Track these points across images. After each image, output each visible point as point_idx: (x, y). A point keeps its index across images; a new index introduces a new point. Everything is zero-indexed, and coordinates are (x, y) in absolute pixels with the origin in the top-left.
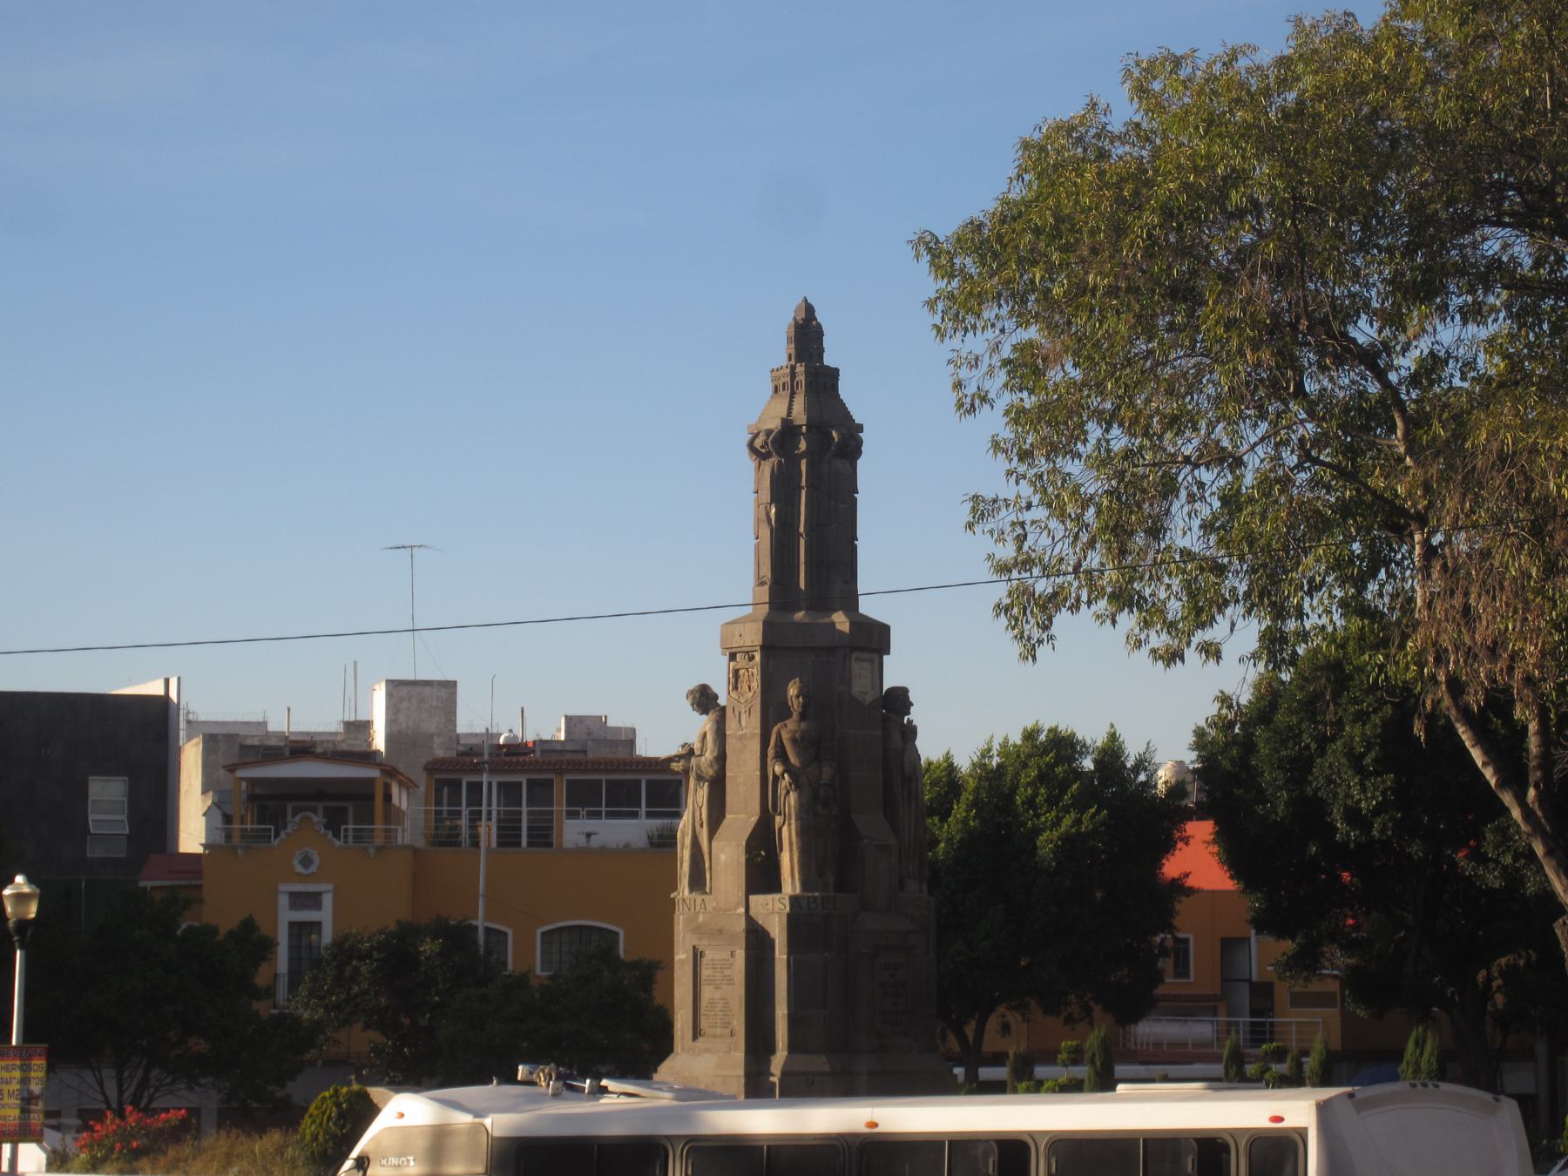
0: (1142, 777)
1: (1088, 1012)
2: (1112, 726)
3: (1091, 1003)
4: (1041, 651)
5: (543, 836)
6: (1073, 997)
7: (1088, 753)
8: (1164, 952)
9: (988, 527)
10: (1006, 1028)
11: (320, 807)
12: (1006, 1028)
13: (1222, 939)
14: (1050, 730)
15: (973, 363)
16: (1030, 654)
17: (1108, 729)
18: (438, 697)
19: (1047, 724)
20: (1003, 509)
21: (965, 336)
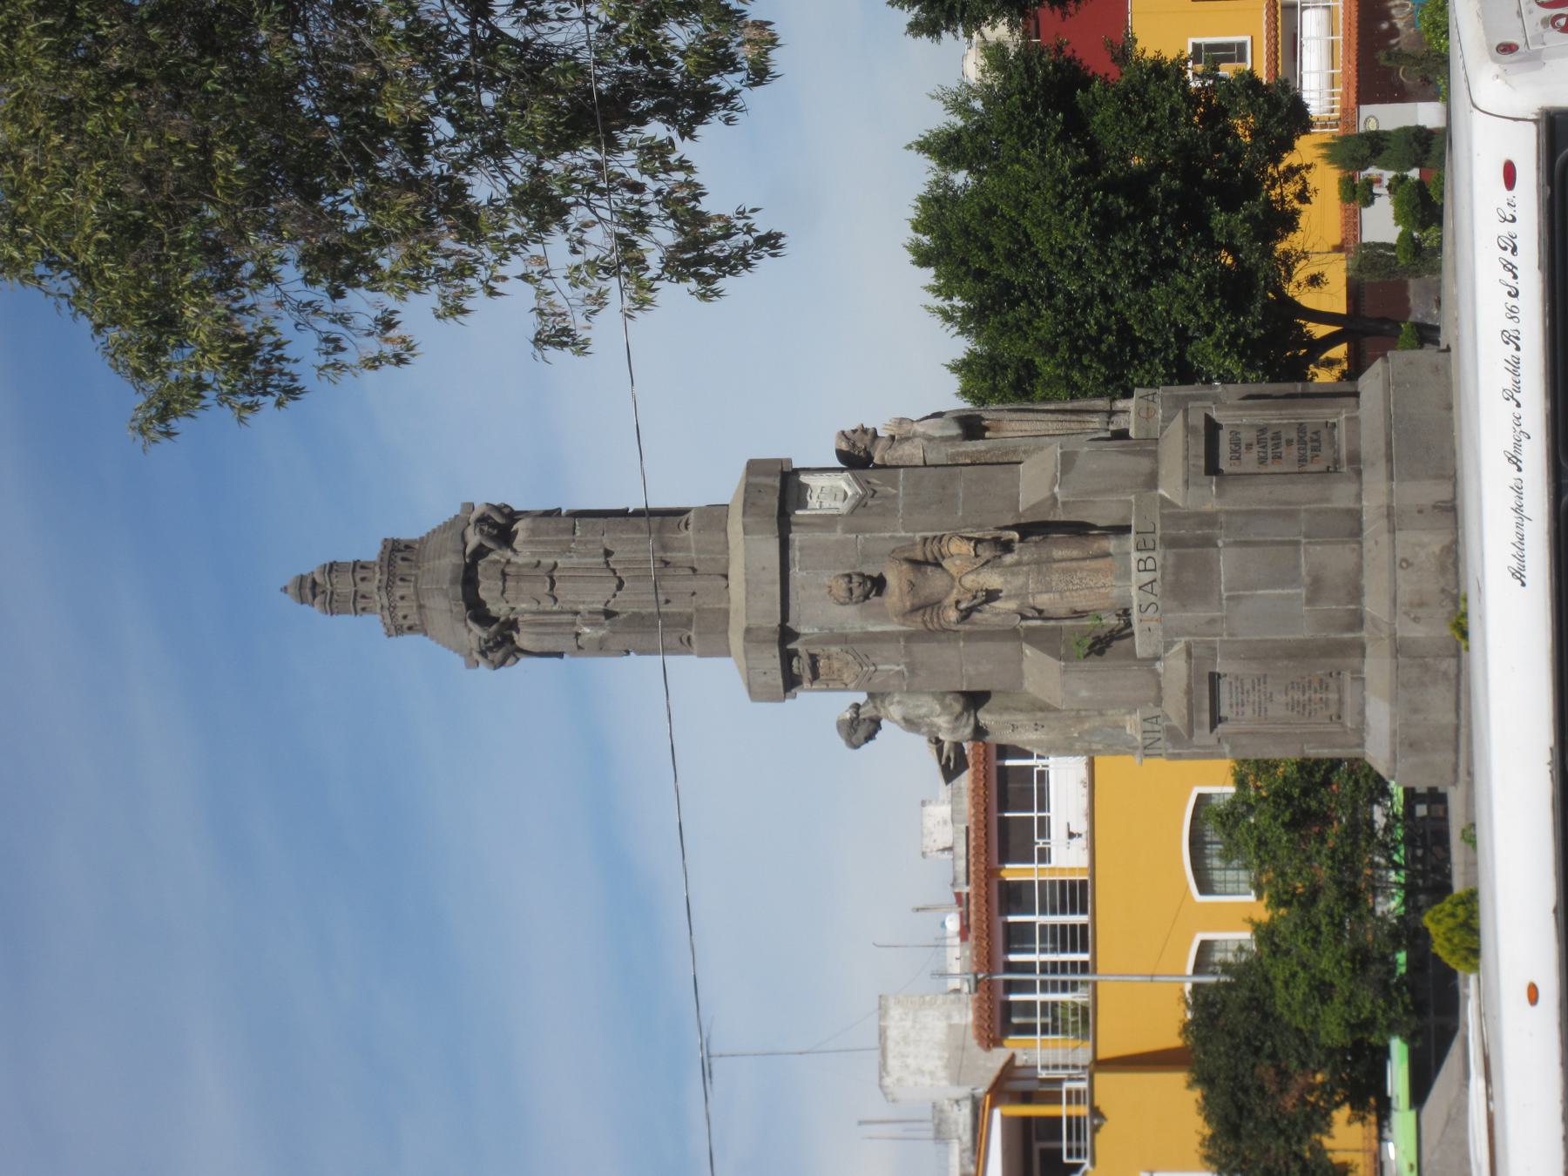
0: (978, 104)
1: (1292, 171)
2: (909, 147)
3: (1282, 167)
5: (1075, 895)
6: (1273, 192)
7: (946, 178)
8: (1211, 73)
9: (581, 321)
10: (1315, 281)
12: (1315, 281)
14: (915, 229)
17: (913, 152)
18: (902, 1019)
19: (908, 235)
20: (555, 298)
21: (288, 360)
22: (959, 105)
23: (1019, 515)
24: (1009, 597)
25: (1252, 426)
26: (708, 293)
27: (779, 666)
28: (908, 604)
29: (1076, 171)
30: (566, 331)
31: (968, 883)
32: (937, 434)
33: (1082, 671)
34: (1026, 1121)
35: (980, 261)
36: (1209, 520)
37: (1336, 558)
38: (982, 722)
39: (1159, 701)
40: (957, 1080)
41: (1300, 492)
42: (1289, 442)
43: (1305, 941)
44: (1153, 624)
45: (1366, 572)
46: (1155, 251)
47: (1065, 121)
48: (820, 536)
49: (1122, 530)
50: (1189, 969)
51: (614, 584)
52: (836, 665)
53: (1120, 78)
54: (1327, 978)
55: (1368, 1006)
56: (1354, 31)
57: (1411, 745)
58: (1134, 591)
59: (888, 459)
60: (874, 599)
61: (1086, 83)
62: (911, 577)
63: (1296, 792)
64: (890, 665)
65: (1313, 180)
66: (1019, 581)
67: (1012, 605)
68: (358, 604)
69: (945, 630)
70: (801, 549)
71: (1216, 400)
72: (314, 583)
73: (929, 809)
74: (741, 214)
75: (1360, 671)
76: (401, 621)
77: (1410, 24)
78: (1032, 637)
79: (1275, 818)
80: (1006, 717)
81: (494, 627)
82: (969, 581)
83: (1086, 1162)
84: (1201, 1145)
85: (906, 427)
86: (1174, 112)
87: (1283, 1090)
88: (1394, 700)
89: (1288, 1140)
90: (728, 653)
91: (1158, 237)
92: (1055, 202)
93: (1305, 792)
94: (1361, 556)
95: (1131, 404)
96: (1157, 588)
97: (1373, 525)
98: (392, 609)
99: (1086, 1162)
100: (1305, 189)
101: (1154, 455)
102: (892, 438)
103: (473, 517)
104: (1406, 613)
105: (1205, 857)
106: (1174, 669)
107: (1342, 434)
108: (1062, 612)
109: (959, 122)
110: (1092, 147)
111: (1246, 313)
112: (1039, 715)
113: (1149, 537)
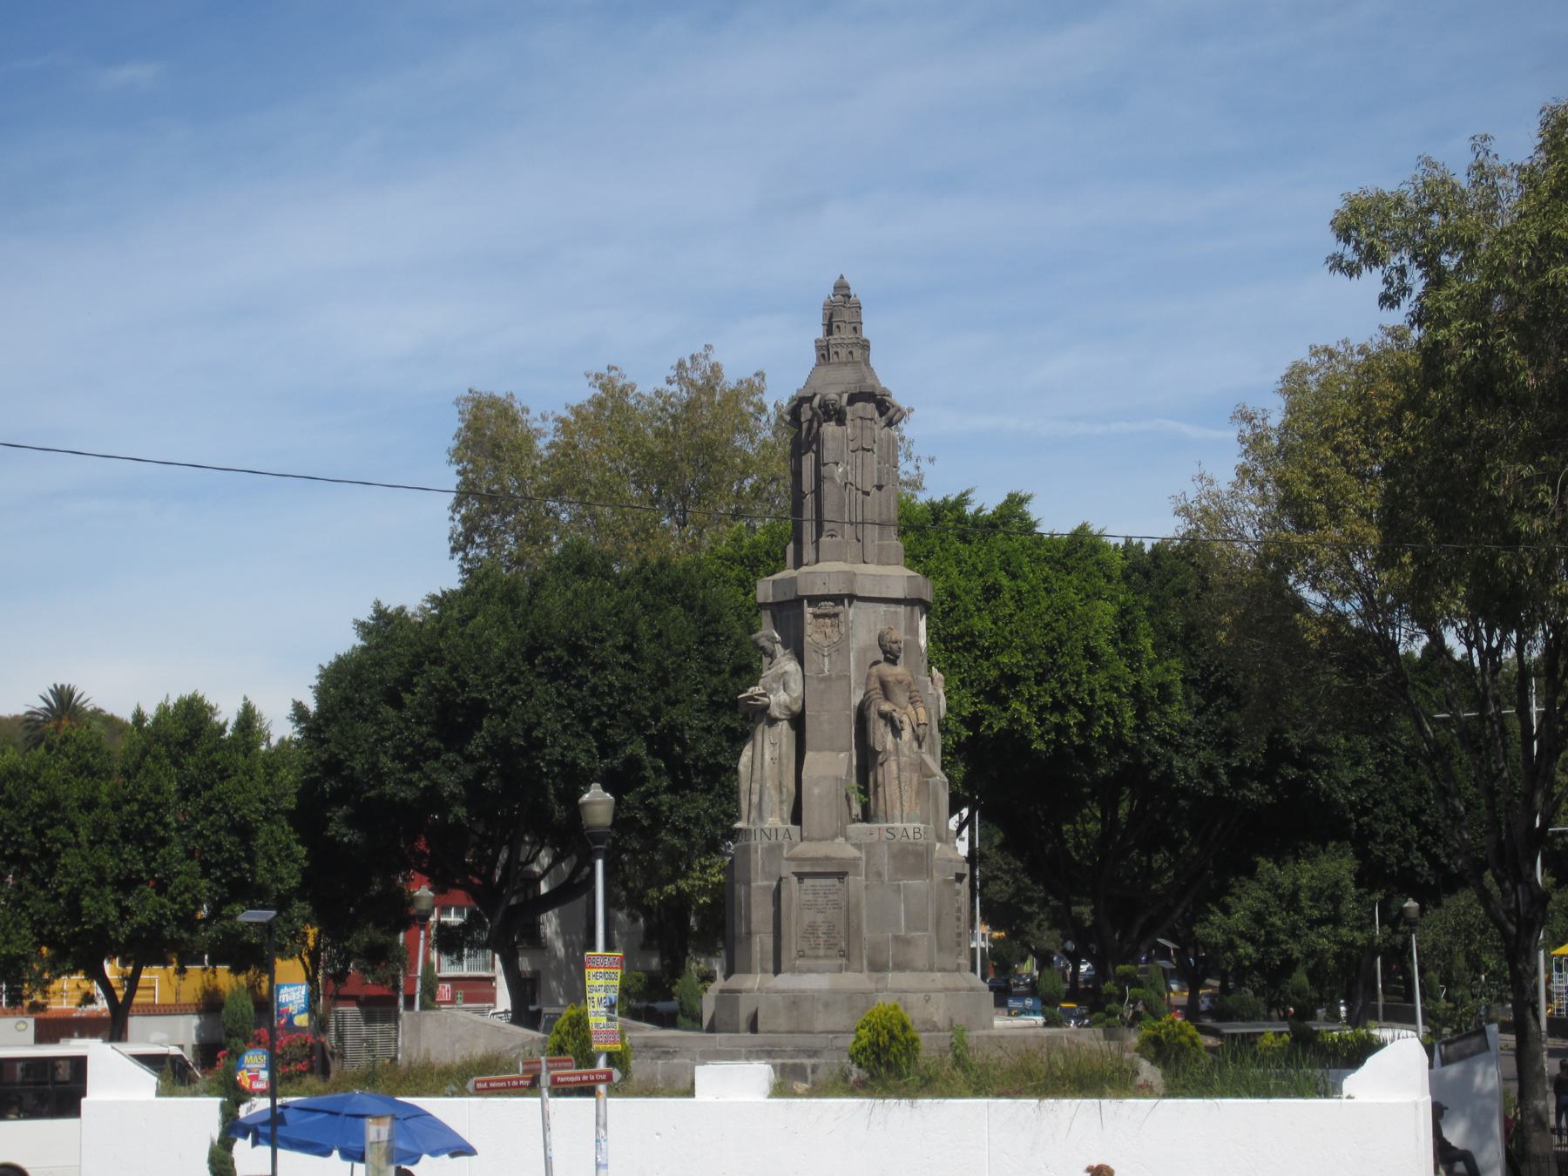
2: (245, 699)
24: (896, 745)
27: (831, 593)
28: (889, 679)
33: (837, 790)
38: (780, 724)
46: (217, 865)
57: (794, 1003)
67: (890, 745)
70: (896, 612)
88: (834, 992)
94: (922, 971)
96: (904, 839)
104: (900, 999)
111: (179, 927)
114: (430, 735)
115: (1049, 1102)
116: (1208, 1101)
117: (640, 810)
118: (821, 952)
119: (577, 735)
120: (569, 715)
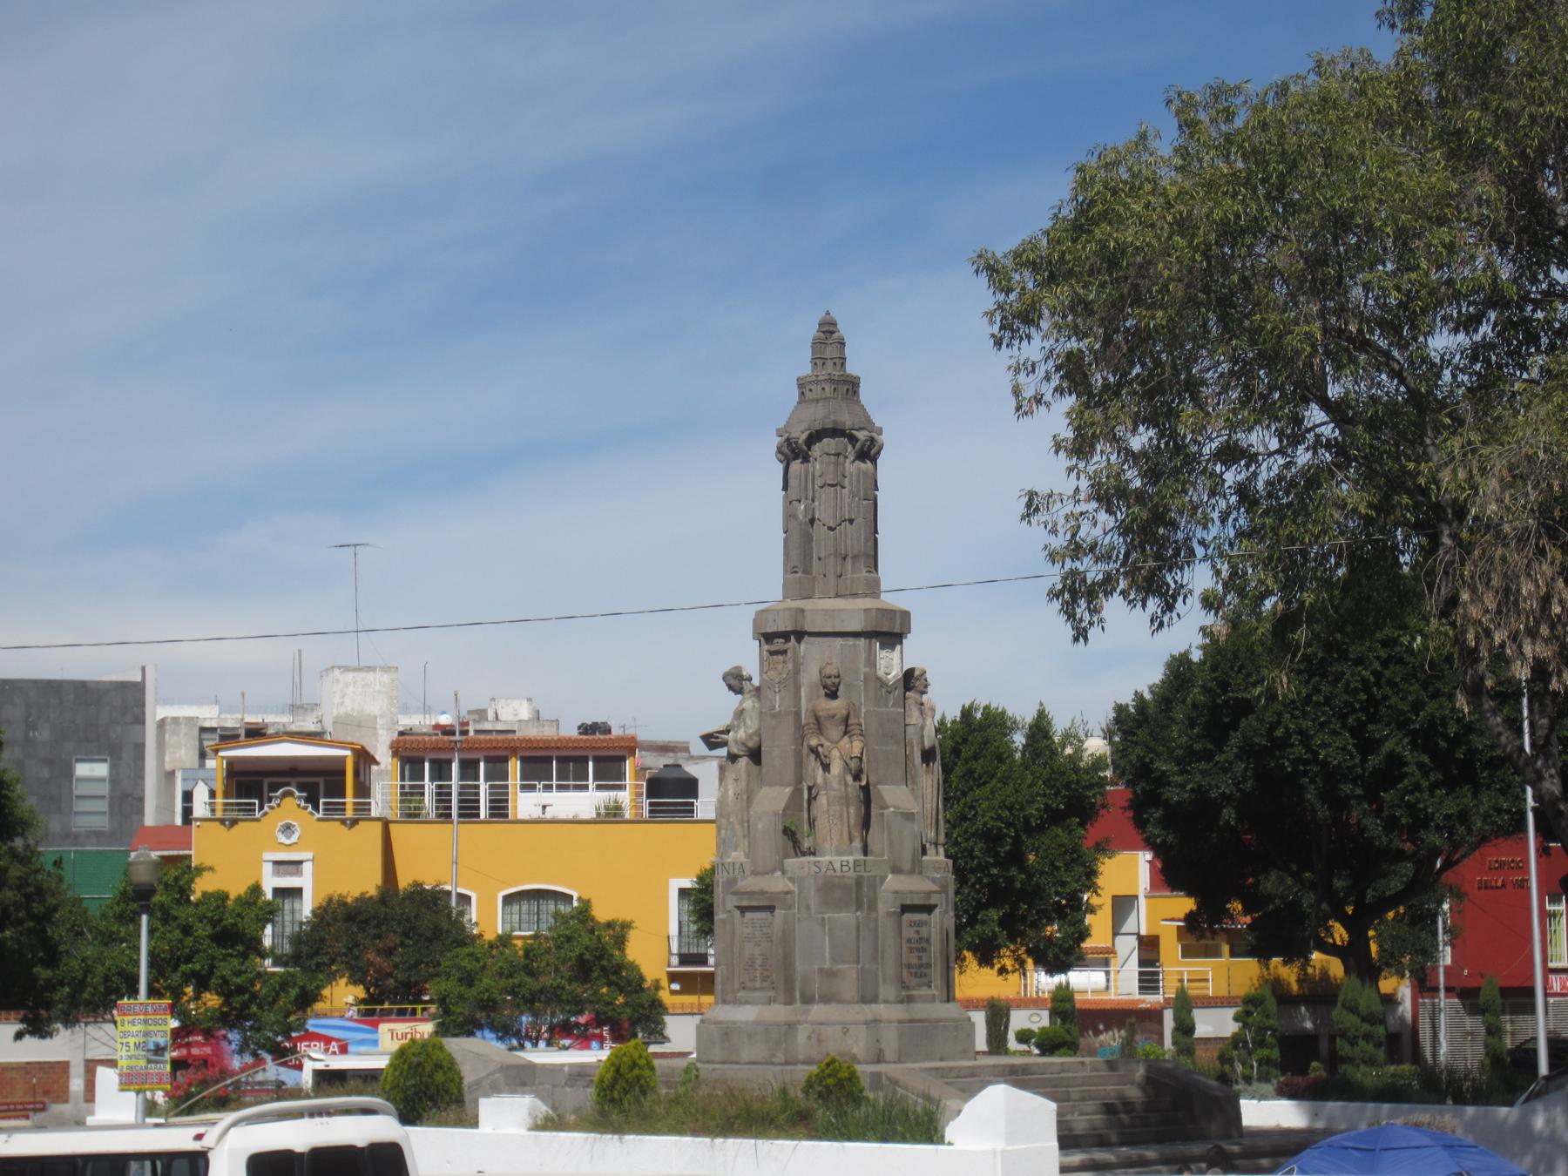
0: (1069, 751)
1: (1022, 963)
2: (1041, 704)
3: (1024, 956)
4: (1093, 633)
5: (499, 809)
9: (1043, 519)
11: (294, 781)
13: (1113, 897)
14: (985, 708)
15: (1030, 369)
16: (1081, 634)
20: (1059, 505)
22: (1068, 737)
23: (875, 786)
24: (825, 778)
25: (930, 933)
26: (1054, 595)
29: (1027, 819)
30: (1037, 510)
31: (477, 732)
32: (926, 733)
34: (343, 773)
35: (966, 752)
36: (873, 906)
37: (848, 987)
39: (754, 873)
40: (336, 722)
41: (889, 965)
42: (920, 958)
43: (501, 968)
44: (806, 870)
45: (840, 1006)
46: (972, 871)
47: (1058, 810)
48: (863, 657)
49: (865, 851)
50: (461, 890)
51: (831, 525)
52: (780, 667)
53: (1086, 846)
54: (476, 983)
55: (459, 1010)
56: (1094, 1007)
57: (726, 1034)
58: (828, 858)
59: (909, 701)
60: (822, 692)
61: (1082, 824)
62: (838, 716)
63: (604, 963)
64: (778, 702)
65: (1014, 978)
66: (835, 785)
67: (820, 780)
68: (818, 361)
69: (803, 737)
71: (946, 911)
72: (832, 332)
73: (525, 704)
74: (1101, 620)
75: (775, 1001)
76: (808, 387)
77: (1102, 1044)
78: (797, 792)
79: (586, 949)
80: (744, 776)
81: (805, 448)
82: (835, 753)
83: (320, 815)
84: (340, 895)
85: (930, 713)
86: (1064, 884)
87: (379, 952)
88: (757, 1023)
89: (345, 955)
90: (785, 597)
91: (983, 872)
92: (1007, 803)
93: (603, 969)
94: (850, 1003)
95: (942, 857)
96: (830, 873)
97: (870, 1011)
98: (817, 382)
99: (318, 816)
100: (1007, 972)
101: (912, 872)
102: (922, 704)
103: (874, 435)
104: (813, 1032)
105: (529, 900)
106: (776, 883)
107: (925, 991)
108: (814, 812)
109: (1056, 739)
110: (1041, 828)
112: (745, 797)
113: (862, 868)
114: (1199, 737)
115: (719, 1141)
116: (835, 1144)
117: (1400, 807)
118: (758, 984)
119: (1334, 733)
120: (1324, 713)
